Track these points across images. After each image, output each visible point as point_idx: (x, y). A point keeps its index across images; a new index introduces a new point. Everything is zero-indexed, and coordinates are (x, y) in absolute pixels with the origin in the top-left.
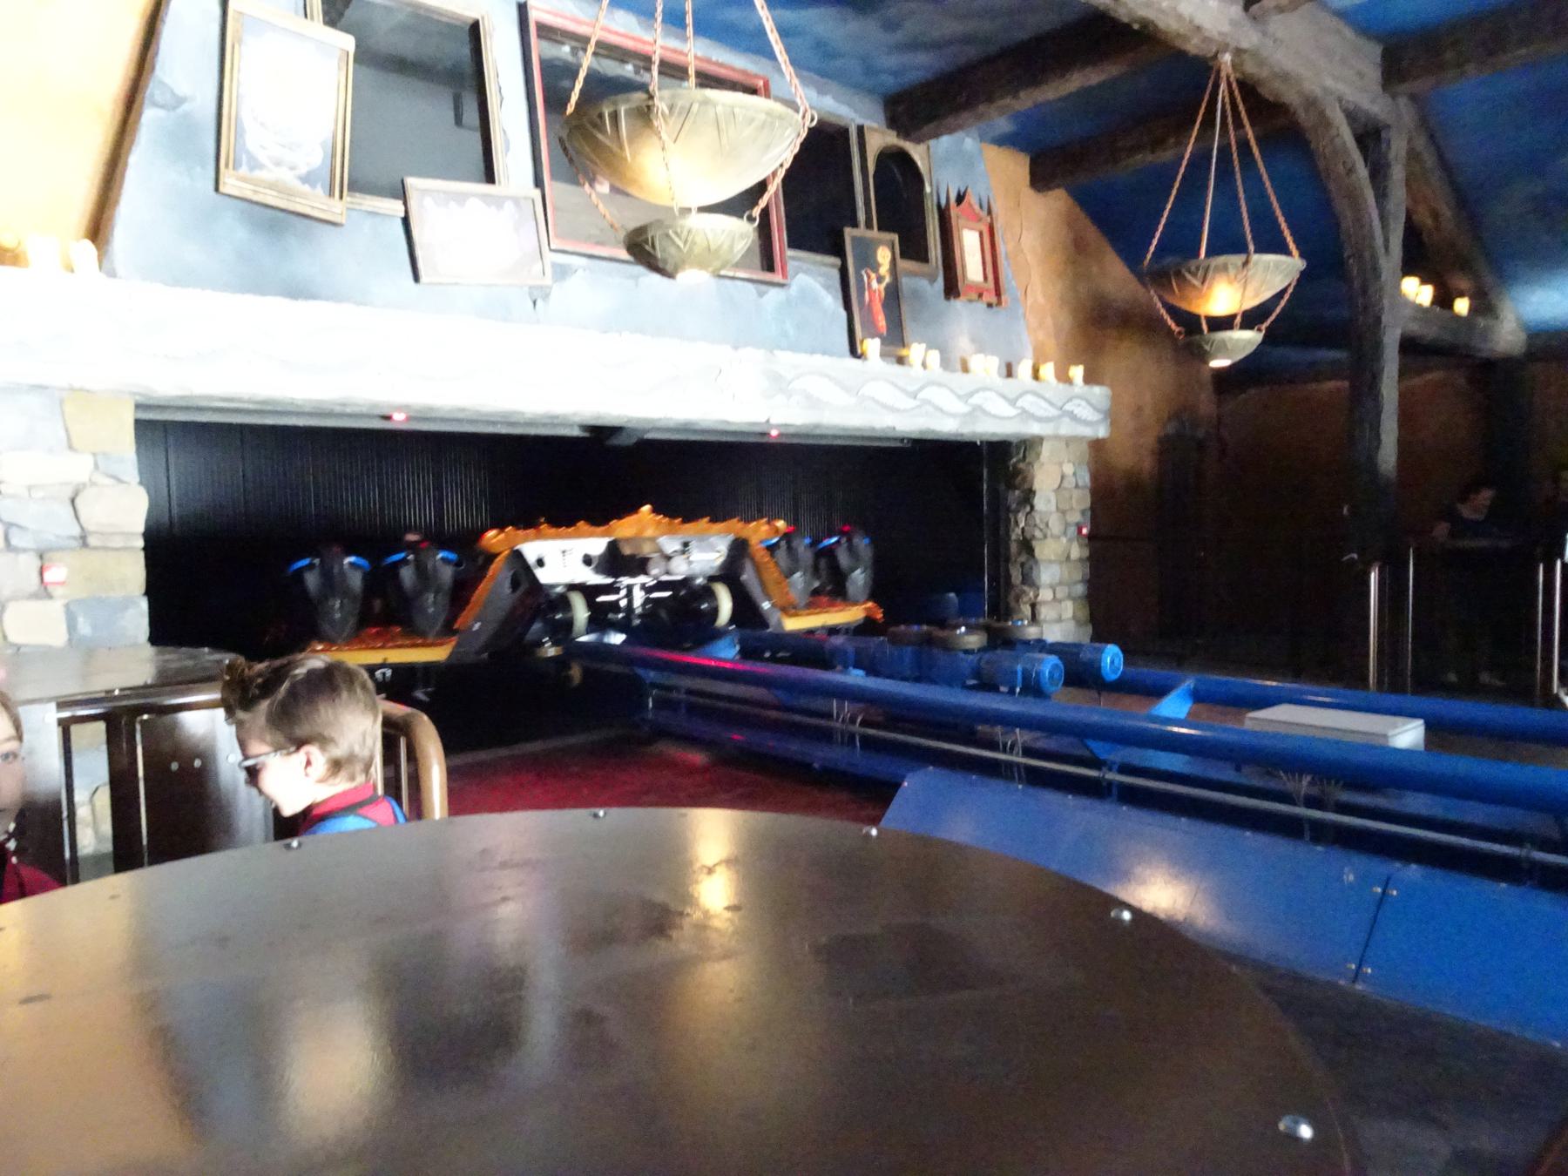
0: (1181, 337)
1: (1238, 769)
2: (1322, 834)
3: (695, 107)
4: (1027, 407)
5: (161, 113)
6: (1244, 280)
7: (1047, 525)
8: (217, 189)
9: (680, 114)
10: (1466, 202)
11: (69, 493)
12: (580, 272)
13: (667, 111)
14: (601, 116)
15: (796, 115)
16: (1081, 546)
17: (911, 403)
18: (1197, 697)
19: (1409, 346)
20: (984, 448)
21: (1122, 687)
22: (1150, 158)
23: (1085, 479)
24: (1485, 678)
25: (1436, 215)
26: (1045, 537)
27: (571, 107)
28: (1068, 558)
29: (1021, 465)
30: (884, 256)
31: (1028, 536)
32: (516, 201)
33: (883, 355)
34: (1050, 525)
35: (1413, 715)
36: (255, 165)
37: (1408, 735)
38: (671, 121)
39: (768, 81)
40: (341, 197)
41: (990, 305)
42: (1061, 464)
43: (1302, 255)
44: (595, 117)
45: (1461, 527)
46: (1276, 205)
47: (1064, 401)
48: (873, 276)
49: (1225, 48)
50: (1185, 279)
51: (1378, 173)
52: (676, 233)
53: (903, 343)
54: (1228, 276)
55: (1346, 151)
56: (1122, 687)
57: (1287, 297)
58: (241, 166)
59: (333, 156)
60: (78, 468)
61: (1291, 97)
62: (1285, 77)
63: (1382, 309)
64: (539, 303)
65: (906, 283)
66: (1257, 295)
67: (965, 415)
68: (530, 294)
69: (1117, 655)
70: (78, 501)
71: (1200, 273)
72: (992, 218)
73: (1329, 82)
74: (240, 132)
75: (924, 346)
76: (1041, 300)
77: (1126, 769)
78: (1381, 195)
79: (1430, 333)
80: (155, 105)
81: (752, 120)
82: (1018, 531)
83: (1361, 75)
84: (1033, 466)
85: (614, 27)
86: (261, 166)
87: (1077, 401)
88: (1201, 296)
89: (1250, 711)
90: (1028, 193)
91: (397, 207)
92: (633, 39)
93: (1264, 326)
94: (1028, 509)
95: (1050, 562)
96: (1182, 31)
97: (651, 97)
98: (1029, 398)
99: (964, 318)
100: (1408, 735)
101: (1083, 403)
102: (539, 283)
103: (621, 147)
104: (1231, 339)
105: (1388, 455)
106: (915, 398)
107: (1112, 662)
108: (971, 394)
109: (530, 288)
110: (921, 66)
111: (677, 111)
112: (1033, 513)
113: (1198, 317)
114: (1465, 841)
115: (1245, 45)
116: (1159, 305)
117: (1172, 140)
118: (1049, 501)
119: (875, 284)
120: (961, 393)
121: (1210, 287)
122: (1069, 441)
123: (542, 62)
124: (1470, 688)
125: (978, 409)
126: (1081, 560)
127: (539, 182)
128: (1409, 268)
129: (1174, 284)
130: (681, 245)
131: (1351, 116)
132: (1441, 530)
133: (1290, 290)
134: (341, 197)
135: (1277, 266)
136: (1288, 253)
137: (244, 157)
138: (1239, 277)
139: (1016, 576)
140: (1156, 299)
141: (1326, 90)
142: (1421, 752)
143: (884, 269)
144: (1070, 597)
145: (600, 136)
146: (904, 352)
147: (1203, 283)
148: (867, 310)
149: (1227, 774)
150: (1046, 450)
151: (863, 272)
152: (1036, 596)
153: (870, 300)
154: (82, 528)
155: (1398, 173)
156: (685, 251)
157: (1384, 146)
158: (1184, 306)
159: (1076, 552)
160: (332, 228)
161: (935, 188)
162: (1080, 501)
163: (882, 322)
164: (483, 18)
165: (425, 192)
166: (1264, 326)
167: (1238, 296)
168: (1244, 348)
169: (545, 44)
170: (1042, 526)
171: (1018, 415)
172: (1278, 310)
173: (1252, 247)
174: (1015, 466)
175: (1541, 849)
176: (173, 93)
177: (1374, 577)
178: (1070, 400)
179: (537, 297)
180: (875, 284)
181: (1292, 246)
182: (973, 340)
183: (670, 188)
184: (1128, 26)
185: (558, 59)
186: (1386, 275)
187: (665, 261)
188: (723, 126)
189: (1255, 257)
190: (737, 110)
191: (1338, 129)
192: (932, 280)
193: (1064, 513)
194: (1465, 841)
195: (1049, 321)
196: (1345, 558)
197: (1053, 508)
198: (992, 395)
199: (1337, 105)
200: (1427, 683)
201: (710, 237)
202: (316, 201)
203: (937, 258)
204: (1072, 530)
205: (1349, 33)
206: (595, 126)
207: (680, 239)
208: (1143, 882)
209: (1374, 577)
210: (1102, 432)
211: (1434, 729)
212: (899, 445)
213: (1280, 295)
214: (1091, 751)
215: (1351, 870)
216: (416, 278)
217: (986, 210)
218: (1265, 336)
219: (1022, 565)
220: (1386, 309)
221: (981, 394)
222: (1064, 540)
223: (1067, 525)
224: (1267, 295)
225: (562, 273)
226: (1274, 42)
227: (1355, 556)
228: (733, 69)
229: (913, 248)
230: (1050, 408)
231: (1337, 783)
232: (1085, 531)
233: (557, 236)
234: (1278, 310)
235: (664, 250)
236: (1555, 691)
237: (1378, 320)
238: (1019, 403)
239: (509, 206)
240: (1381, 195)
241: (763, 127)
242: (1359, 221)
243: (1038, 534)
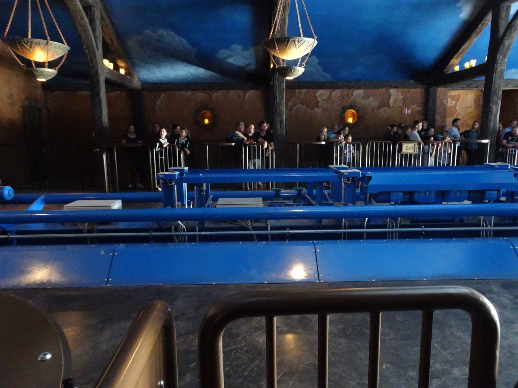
1: (63, 225)
2: (93, 241)
6: (47, 50)
10: (121, 37)
18: (46, 202)
19: (108, 82)
21: (14, 202)
24: (139, 185)
25: (112, 40)
35: (117, 198)
37: (117, 205)
43: (68, 45)
45: (129, 140)
46: (55, 21)
51: (92, 21)
54: (40, 46)
55: (80, 11)
56: (14, 202)
57: (64, 59)
63: (98, 69)
66: (53, 56)
69: (10, 190)
71: (29, 44)
77: (18, 233)
78: (94, 30)
79: (114, 78)
88: (32, 54)
89: (65, 205)
100: (117, 205)
104: (45, 71)
105: (105, 119)
107: (8, 193)
113: (30, 61)
114: (135, 234)
116: (13, 54)
121: (34, 50)
124: (135, 189)
128: (105, 57)
132: (124, 141)
140: (11, 51)
142: (121, 209)
147: (31, 48)
149: (60, 227)
155: (98, 23)
157: (93, 12)
166: (57, 68)
172: (62, 63)
173: (49, 38)
175: (155, 232)
177: (104, 156)
181: (64, 41)
186: (100, 60)
189: (50, 42)
194: (135, 234)
200: (124, 188)
208: (29, 272)
209: (104, 156)
211: (125, 203)
213: (61, 58)
214: (3, 229)
215: (103, 250)
218: (58, 72)
220: (99, 69)
224: (57, 57)
227: (98, 150)
231: (97, 224)
234: (62, 63)
236: (156, 187)
237: (97, 72)
240: (94, 30)
242: (87, 36)
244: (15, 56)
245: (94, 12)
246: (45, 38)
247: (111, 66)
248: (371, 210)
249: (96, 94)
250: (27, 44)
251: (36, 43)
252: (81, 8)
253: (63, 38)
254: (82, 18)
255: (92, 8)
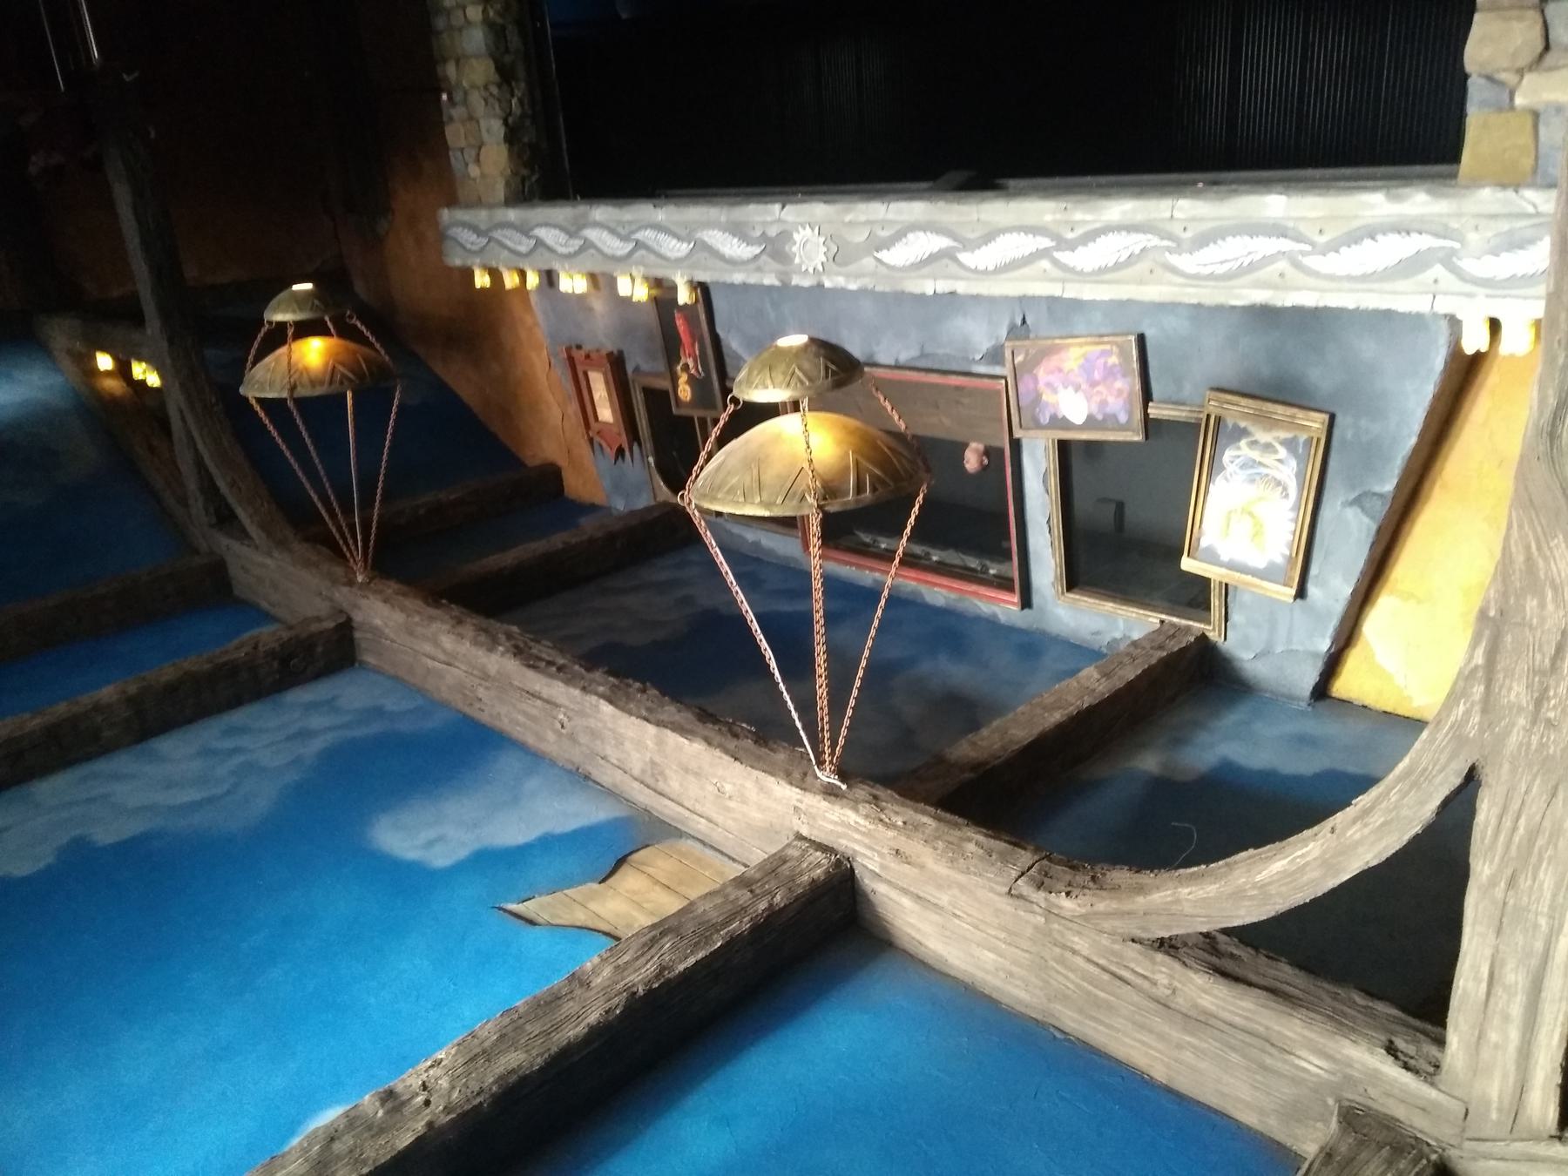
0: (348, 313)
3: (779, 501)
4: (524, 240)
5: (1377, 489)
6: (292, 372)
7: (486, 100)
8: (1332, 417)
9: (795, 493)
11: (1550, 59)
12: (978, 357)
13: (807, 495)
14: (874, 489)
15: (697, 503)
16: (446, 79)
17: (640, 235)
19: (138, 320)
20: (571, 191)
22: (442, 496)
23: (455, 160)
26: (486, 88)
27: (919, 502)
28: (458, 62)
29: (525, 172)
30: (685, 392)
31: (505, 87)
32: (1038, 426)
33: (674, 288)
34: (483, 103)
36: (1290, 445)
38: (804, 487)
39: (805, 551)
40: (1208, 416)
41: (579, 347)
42: (483, 176)
43: (246, 399)
44: (880, 490)
47: (487, 248)
48: (693, 371)
49: (362, 586)
50: (352, 371)
52: (802, 383)
53: (656, 300)
57: (251, 358)
58: (1306, 441)
59: (1212, 458)
60: (1533, 92)
61: (300, 548)
62: (308, 564)
64: (1019, 322)
65: (661, 366)
66: (277, 360)
67: (584, 226)
68: (1028, 330)
70: (1540, 47)
72: (588, 435)
73: (269, 561)
74: (1300, 476)
75: (635, 299)
76: (533, 355)
78: (200, 464)
80: (1381, 496)
81: (728, 492)
82: (518, 93)
83: (246, 571)
84: (512, 171)
85: (944, 591)
86: (1285, 443)
87: (474, 248)
90: (562, 462)
91: (1153, 411)
92: (927, 582)
93: (267, 326)
94: (510, 120)
95: (477, 57)
96: (401, 598)
97: (820, 507)
98: (523, 249)
99: (600, 332)
101: (469, 246)
102: (1018, 343)
103: (857, 463)
104: (294, 312)
106: (637, 242)
108: (582, 249)
109: (1027, 338)
110: (660, 571)
111: (798, 497)
112: (504, 115)
115: (345, 590)
116: (378, 346)
117: (422, 511)
118: (488, 131)
119: (691, 364)
120: (592, 251)
121: (326, 364)
122: (478, 203)
123: (1010, 558)
125: (572, 234)
126: (445, 60)
127: (1016, 445)
129: (364, 366)
130: (797, 370)
131: (243, 535)
133: (249, 364)
134: (1208, 416)
135: (262, 389)
136: (259, 400)
137: (1301, 450)
138: (296, 376)
139: (514, 40)
141: (270, 555)
143: (683, 378)
144: (448, 12)
145: (877, 472)
146: (654, 292)
148: (695, 336)
150: (500, 192)
151: (703, 374)
152: (485, 11)
153: (693, 345)
154: (1542, 12)
155: (192, 485)
156: (794, 366)
157: (212, 510)
158: (352, 346)
159: (451, 70)
160: (1224, 385)
161: (646, 461)
162: (455, 134)
163: (680, 323)
164: (1063, 593)
165: (1123, 428)
167: (295, 357)
168: (279, 304)
169: (1009, 574)
170: (491, 100)
171: (532, 229)
173: (290, 404)
174: (533, 171)
176: (1363, 509)
178: (482, 250)
179: (1020, 330)
180: (691, 364)
181: (257, 408)
182: (591, 309)
183: (806, 425)
184: (451, 601)
185: (942, 550)
187: (817, 355)
188: (755, 485)
189: (285, 395)
190: (741, 499)
191: (252, 522)
192: (637, 369)
193: (471, 118)
195: (523, 334)
196: (136, 74)
197: (482, 123)
198: (562, 250)
199: (257, 542)
201: (769, 382)
202: (1236, 411)
203: (635, 392)
204: (458, 97)
205: (264, 605)
206: (883, 482)
207: (799, 378)
210: (445, 215)
212: (669, 192)
216: (1141, 340)
217: (595, 442)
219: (507, 51)
221: (571, 250)
222: (465, 84)
223: (465, 102)
224: (268, 359)
225: (995, 356)
226: (321, 594)
228: (836, 560)
229: (659, 400)
230: (500, 238)
232: (444, 97)
233: (998, 393)
235: (817, 366)
237: (171, 342)
238: (533, 242)
239: (1045, 419)
240: (200, 464)
241: (720, 488)
243: (494, 90)
244: (372, 339)
245: (206, 510)
246: (299, 402)
247: (140, 370)
248: (1135, 610)
249: (167, 273)
250: (343, 375)
251: (322, 383)
252: (241, 513)
253: (262, 414)
254: (232, 486)
255: (214, 520)
